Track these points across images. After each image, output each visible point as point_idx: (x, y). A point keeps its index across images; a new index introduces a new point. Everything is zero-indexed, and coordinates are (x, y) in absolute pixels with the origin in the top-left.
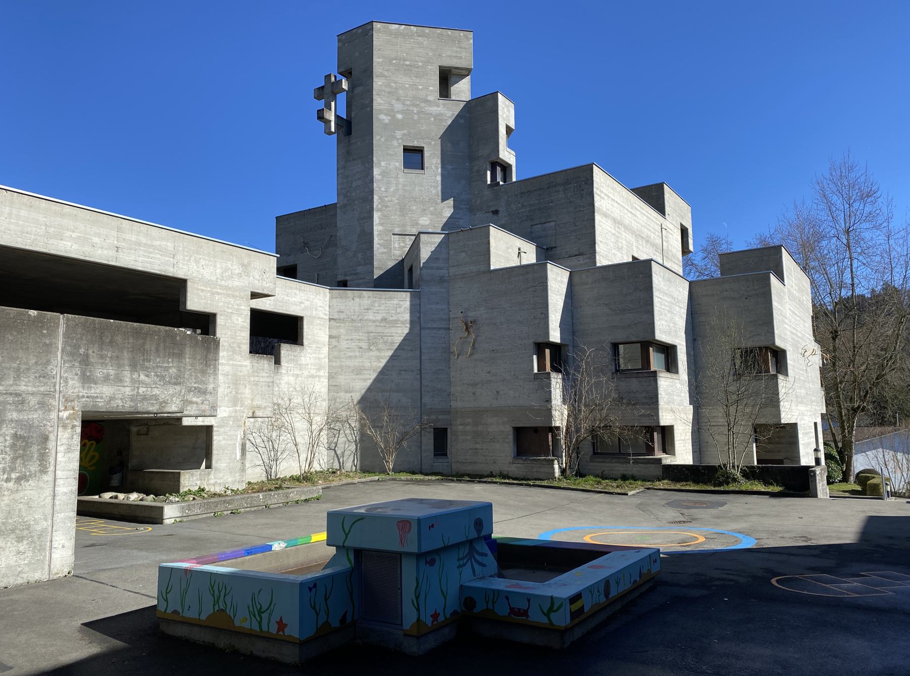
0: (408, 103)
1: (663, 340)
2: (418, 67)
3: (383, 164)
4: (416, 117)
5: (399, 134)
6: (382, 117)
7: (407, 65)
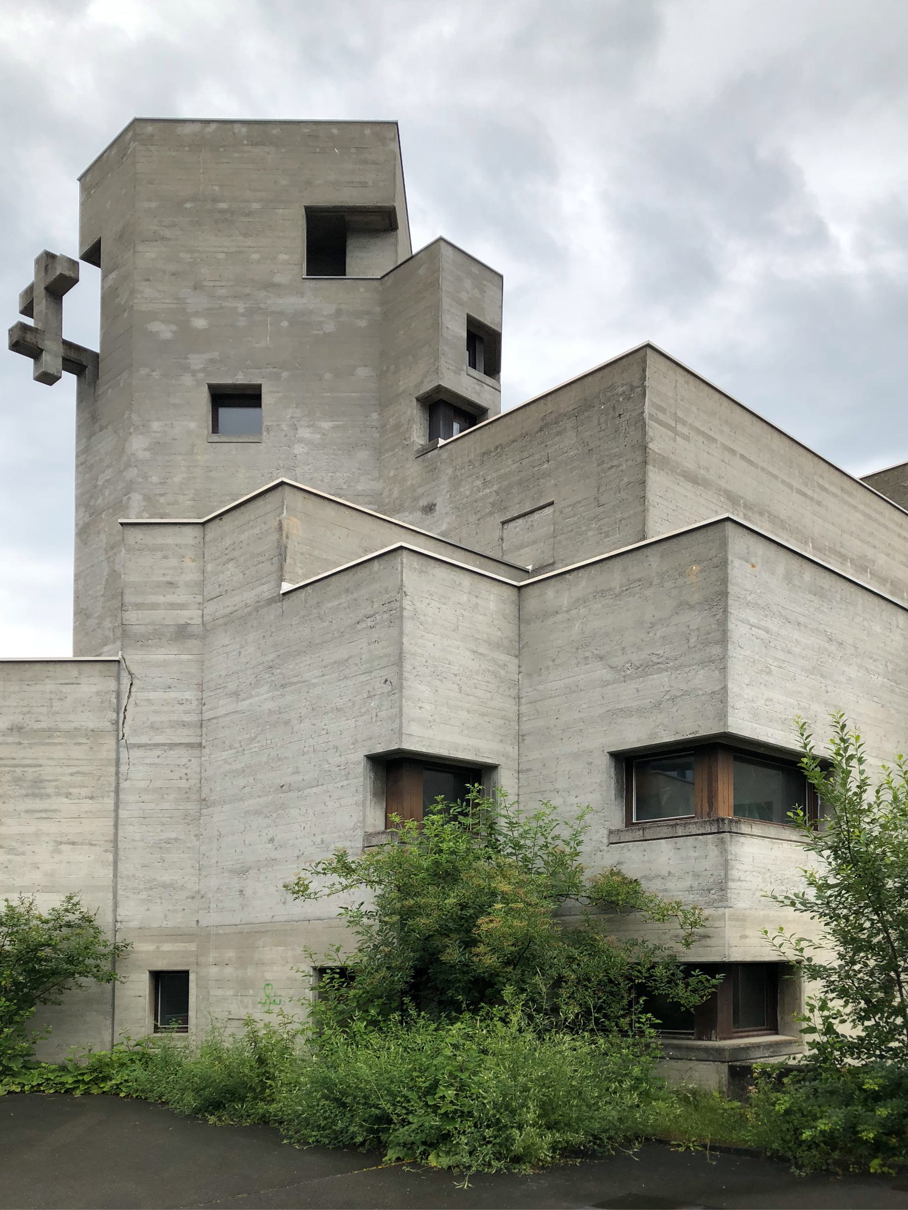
0: (223, 292)
1: (772, 741)
2: (249, 214)
3: (156, 426)
4: (242, 322)
5: (196, 361)
6: (156, 327)
7: (222, 211)
